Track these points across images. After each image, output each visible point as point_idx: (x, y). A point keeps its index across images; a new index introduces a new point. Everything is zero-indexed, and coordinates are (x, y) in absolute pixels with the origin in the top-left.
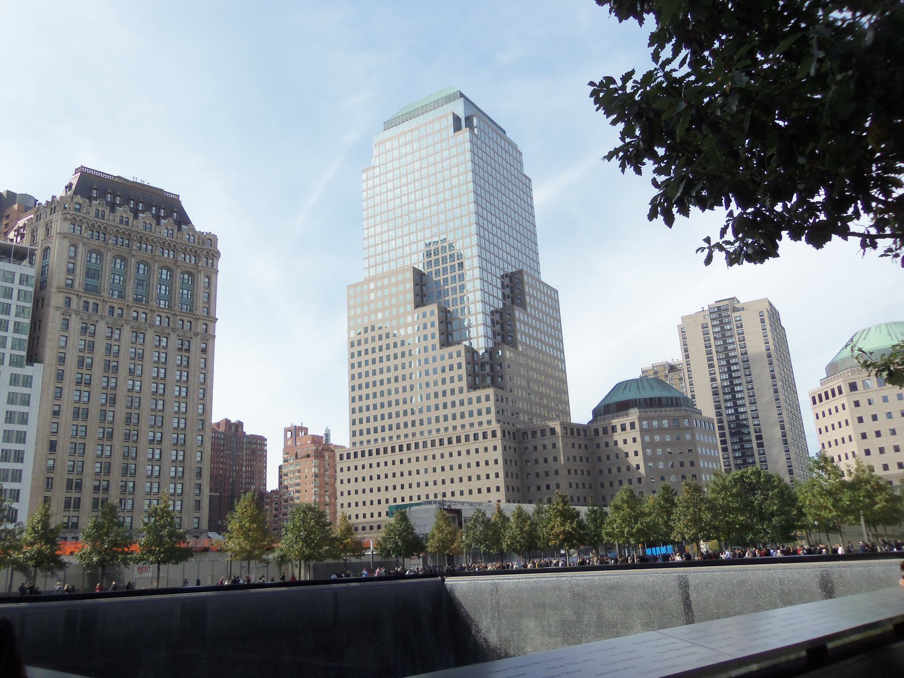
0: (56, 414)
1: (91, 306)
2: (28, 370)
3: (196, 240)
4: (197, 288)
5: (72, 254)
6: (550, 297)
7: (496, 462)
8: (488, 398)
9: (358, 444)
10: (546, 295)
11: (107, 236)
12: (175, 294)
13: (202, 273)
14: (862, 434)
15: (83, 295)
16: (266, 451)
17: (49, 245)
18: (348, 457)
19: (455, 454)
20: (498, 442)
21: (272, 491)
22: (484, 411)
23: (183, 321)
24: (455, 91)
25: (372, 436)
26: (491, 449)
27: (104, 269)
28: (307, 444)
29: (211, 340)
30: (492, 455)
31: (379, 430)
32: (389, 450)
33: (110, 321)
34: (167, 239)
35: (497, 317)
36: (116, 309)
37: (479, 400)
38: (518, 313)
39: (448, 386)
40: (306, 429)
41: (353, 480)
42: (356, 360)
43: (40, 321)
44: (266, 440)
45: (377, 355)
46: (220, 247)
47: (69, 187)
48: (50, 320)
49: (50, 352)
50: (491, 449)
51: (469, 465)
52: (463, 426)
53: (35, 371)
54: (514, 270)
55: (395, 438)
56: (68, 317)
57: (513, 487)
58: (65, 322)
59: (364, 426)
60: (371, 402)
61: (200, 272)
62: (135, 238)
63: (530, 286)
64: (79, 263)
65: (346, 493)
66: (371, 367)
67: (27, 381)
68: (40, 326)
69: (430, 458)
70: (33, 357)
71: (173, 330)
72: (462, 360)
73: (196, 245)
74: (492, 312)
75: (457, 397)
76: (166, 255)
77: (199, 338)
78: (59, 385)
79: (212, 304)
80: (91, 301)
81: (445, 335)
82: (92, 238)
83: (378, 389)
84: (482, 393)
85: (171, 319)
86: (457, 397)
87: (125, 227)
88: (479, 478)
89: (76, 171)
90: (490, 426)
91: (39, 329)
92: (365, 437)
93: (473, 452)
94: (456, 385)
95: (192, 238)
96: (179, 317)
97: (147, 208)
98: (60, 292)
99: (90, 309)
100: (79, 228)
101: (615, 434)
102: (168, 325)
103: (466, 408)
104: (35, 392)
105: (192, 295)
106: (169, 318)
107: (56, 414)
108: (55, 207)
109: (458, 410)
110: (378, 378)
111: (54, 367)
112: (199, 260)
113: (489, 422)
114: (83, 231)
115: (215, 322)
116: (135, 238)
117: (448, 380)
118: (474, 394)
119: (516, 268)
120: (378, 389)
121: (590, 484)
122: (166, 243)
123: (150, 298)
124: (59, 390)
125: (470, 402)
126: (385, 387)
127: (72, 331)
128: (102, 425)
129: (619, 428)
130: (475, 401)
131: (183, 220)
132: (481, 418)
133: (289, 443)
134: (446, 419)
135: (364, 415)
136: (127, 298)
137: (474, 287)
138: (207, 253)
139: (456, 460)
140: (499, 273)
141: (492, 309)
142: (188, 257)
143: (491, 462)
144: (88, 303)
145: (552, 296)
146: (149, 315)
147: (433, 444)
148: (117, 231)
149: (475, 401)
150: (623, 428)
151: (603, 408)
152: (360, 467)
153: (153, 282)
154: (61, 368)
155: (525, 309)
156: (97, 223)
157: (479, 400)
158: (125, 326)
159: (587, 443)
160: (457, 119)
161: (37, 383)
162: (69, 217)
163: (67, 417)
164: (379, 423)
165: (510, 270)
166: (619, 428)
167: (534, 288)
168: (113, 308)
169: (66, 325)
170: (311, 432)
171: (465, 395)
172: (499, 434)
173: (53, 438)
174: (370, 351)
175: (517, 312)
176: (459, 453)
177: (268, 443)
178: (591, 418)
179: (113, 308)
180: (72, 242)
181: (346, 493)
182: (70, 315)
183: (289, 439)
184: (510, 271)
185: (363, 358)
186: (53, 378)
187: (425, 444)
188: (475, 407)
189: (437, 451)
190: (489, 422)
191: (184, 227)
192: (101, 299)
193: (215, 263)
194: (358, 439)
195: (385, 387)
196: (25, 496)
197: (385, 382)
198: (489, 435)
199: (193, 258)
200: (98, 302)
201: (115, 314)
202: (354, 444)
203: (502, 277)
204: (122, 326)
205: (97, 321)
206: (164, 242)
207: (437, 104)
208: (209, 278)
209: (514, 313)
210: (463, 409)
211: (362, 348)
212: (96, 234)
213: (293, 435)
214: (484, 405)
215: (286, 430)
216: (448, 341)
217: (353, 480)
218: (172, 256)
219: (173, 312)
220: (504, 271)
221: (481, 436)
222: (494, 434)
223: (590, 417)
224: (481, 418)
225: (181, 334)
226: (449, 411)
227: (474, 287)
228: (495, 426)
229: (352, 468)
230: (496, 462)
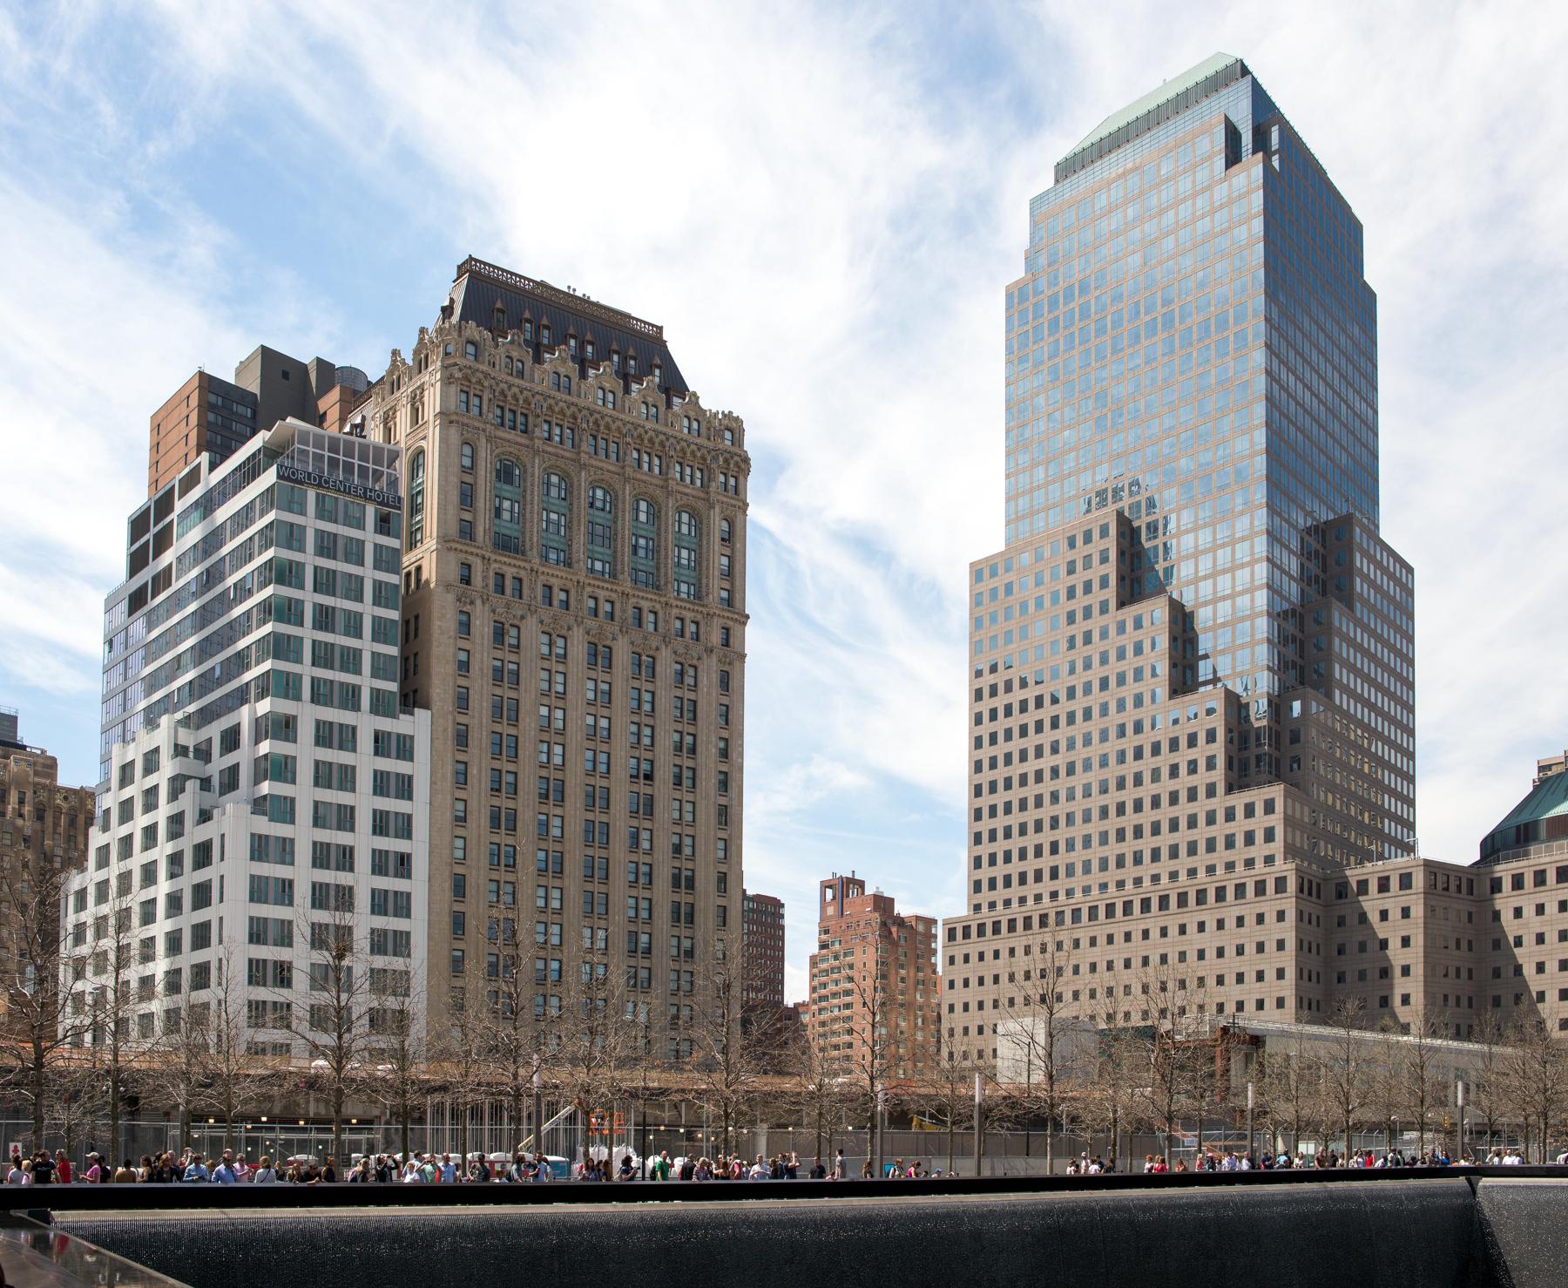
0: (461, 820)
1: (508, 582)
2: (400, 725)
3: (703, 431)
4: (708, 543)
5: (467, 462)
6: (1398, 582)
7: (1281, 945)
8: (1269, 807)
9: (985, 909)
10: (1392, 576)
11: (530, 419)
12: (666, 557)
13: (717, 509)
14: (1408, 975)
15: (493, 557)
16: (782, 928)
17: (423, 443)
18: (966, 935)
19: (1192, 928)
20: (1289, 904)
21: (797, 1006)
22: (1259, 836)
23: (640, 609)
24: (1230, 61)
25: (1015, 891)
26: (1270, 918)
27: (528, 498)
28: (864, 912)
29: (737, 664)
30: (1273, 931)
31: (1030, 877)
32: (1020, 924)
33: (546, 614)
34: (648, 425)
35: (1291, 628)
36: (556, 590)
37: (1249, 811)
38: (1338, 618)
39: (1184, 781)
40: (861, 884)
41: (973, 982)
42: (987, 728)
43: (417, 617)
44: (783, 906)
45: (1030, 718)
46: (750, 444)
47: (447, 311)
48: (436, 614)
49: (441, 680)
50: (1270, 918)
51: (1220, 953)
52: (1138, 881)
53: (417, 725)
54: (1331, 517)
55: (1015, 904)
56: (467, 608)
57: (1310, 1000)
58: (464, 618)
59: (1000, 870)
60: (1014, 819)
61: (712, 507)
62: (584, 426)
63: (1365, 554)
64: (481, 482)
65: (959, 1008)
66: (1016, 745)
67: (404, 747)
68: (416, 629)
69: (1137, 936)
70: (411, 698)
71: (666, 640)
72: (1218, 723)
73: (701, 441)
74: (1286, 612)
75: (1202, 806)
76: (646, 467)
77: (714, 658)
78: (461, 757)
79: (738, 583)
80: (510, 572)
81: (1180, 668)
82: (502, 425)
83: (1031, 791)
84: (1257, 796)
85: (661, 614)
86: (1202, 806)
87: (565, 397)
88: (1260, 976)
89: (461, 270)
90: (1272, 869)
91: (416, 635)
92: (1001, 894)
93: (1230, 923)
94: (1202, 778)
95: (695, 425)
96: (675, 611)
97: (604, 355)
98: (450, 549)
99: (508, 591)
100: (476, 401)
101: (1497, 895)
102: (656, 630)
103: (1220, 830)
104: (420, 769)
105: (698, 562)
106: (655, 613)
107: (461, 820)
108: (427, 357)
109: (1202, 833)
110: (1031, 766)
111: (450, 717)
112: (709, 480)
113: (1269, 860)
114: (485, 407)
115: (744, 624)
116: (584, 426)
117: (1183, 769)
118: (1239, 800)
119: (1335, 513)
120: (1031, 791)
121: (1470, 999)
122: (646, 437)
123: (619, 567)
124: (462, 767)
125: (1230, 815)
126: (1046, 788)
127: (478, 641)
128: (543, 845)
129: (1507, 884)
130: (1240, 813)
131: (673, 385)
132: (1253, 852)
133: (830, 911)
134: (1138, 859)
135: (1000, 846)
136: (576, 565)
137: (1252, 554)
138: (726, 461)
139: (1194, 941)
140: (1302, 521)
141: (1286, 606)
142: (688, 471)
143: (1271, 946)
144: (503, 576)
145: (1401, 574)
146: (618, 606)
147: (1146, 905)
148: (550, 408)
149: (1240, 813)
150: (1518, 882)
151: (1513, 831)
152: (989, 956)
153: (623, 529)
154: (462, 719)
155: (1351, 608)
156: (510, 387)
157: (1249, 811)
158: (575, 629)
159: (1473, 909)
160: (1232, 134)
161: (422, 749)
162: (458, 375)
163: (479, 826)
164: (1031, 865)
165: (1325, 515)
166: (1507, 884)
167: (1372, 559)
168: (550, 588)
169: (465, 627)
170: (870, 890)
171: (1220, 803)
172: (1292, 885)
173: (459, 870)
174: (1016, 708)
175: (1336, 615)
176: (1201, 927)
177: (788, 912)
178: (1478, 858)
179: (550, 588)
180: (467, 435)
181: (959, 1008)
182: (472, 603)
183: (830, 904)
184: (1324, 518)
185: (1002, 724)
186: (449, 743)
187: (1164, 902)
188: (1240, 826)
189: (1154, 922)
190: (1269, 860)
191: (676, 400)
192: (528, 566)
193: (741, 487)
194: (985, 896)
195: (1046, 788)
196: (419, 982)
197: (1031, 778)
198: (1270, 886)
199: (698, 474)
200: (522, 574)
201: (555, 602)
202: (977, 908)
203: (1308, 531)
204: (569, 629)
205: (522, 617)
206: (640, 436)
207: (1183, 102)
208: (731, 524)
209: (1330, 617)
210: (1193, 835)
211: (999, 702)
212: (508, 415)
213: (839, 895)
214: (1260, 822)
215: (825, 885)
216: (1185, 683)
217: (973, 982)
218: (657, 470)
219: (663, 599)
220: (1314, 519)
221: (1250, 890)
222: (1280, 884)
223: (1476, 856)
224: (1253, 852)
225: (681, 650)
226: (1183, 836)
227: (1252, 554)
228: (1285, 868)
229: (974, 958)
230: (1281, 945)
